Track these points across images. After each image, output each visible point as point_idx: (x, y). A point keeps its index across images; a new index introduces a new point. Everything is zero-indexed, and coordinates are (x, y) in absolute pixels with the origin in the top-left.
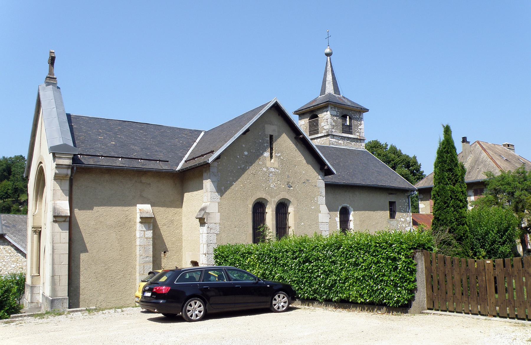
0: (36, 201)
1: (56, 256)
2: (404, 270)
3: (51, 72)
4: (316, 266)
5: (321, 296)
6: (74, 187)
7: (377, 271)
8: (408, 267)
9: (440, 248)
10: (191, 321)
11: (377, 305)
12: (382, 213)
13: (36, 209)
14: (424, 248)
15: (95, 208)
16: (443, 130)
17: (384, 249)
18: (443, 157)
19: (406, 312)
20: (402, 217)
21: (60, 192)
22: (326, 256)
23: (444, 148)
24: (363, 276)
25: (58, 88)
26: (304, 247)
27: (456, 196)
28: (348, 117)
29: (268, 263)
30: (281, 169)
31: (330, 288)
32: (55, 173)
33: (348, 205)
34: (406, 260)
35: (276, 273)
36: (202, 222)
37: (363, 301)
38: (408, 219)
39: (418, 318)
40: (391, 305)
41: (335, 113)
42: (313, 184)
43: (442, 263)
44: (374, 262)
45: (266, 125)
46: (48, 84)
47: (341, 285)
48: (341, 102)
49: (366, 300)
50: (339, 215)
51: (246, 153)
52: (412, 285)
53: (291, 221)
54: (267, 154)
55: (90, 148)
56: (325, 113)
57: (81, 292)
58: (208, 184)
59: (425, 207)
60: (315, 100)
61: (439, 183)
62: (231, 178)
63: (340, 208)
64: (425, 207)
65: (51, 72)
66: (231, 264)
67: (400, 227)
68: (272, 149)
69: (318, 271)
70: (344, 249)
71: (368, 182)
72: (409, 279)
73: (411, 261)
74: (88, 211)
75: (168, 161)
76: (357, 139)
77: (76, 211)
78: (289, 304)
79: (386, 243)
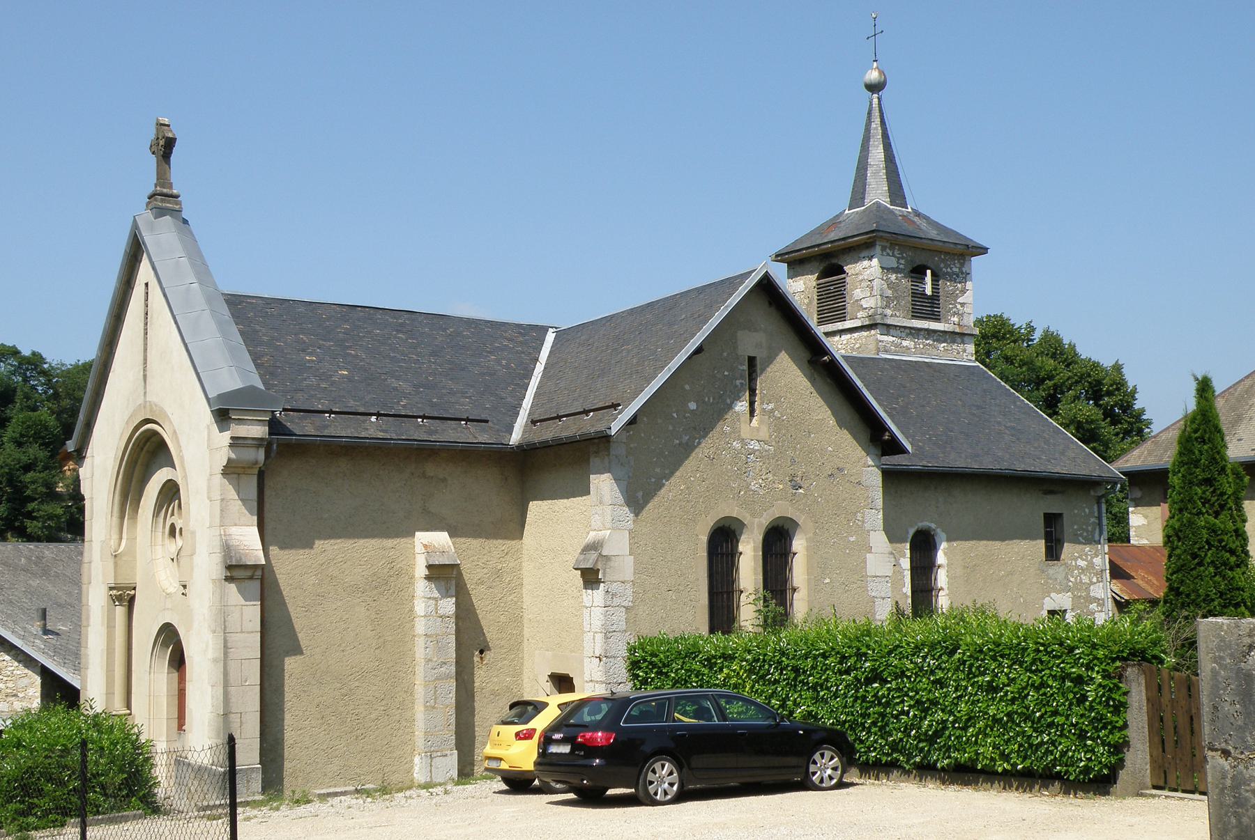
0: (122, 517)
1: (232, 665)
2: (1100, 703)
3: (163, 177)
4: (898, 689)
5: (909, 757)
6: (268, 493)
7: (1041, 704)
8: (1109, 698)
9: (1182, 656)
10: (655, 803)
11: (1041, 777)
12: (1025, 544)
13: (121, 538)
14: (1144, 659)
15: (317, 542)
16: (1192, 387)
17: (1054, 657)
18: (1192, 452)
19: (1106, 793)
20: (1080, 557)
21: (237, 506)
22: (921, 669)
23: (1196, 431)
24: (1009, 715)
25: (185, 222)
26: (868, 647)
27: (1221, 541)
28: (929, 272)
29: (776, 682)
30: (779, 446)
31: (931, 740)
32: (229, 460)
33: (933, 526)
34: (1105, 682)
35: (796, 704)
36: (591, 578)
37: (1009, 768)
38: (1097, 561)
39: (1131, 802)
40: (1072, 778)
41: (893, 262)
42: (852, 479)
43: (1184, 691)
44: (1033, 685)
45: (740, 334)
46: (160, 212)
47: (958, 733)
48: (908, 229)
49: (1014, 765)
50: (908, 552)
51: (692, 406)
52: (1118, 735)
53: (799, 572)
54: (742, 406)
55: (296, 390)
56: (866, 263)
57: (286, 754)
58: (603, 485)
59: (1146, 525)
60: (834, 223)
61: (1181, 510)
62: (658, 470)
63: (912, 532)
64: (1146, 525)
65: (163, 177)
66: (676, 683)
67: (1075, 583)
68: (753, 392)
69: (903, 701)
70: (964, 654)
71: (987, 463)
72: (1111, 723)
73: (1115, 685)
74: (301, 551)
75: (487, 421)
76: (953, 333)
77: (274, 550)
78: (843, 772)
79: (1061, 644)
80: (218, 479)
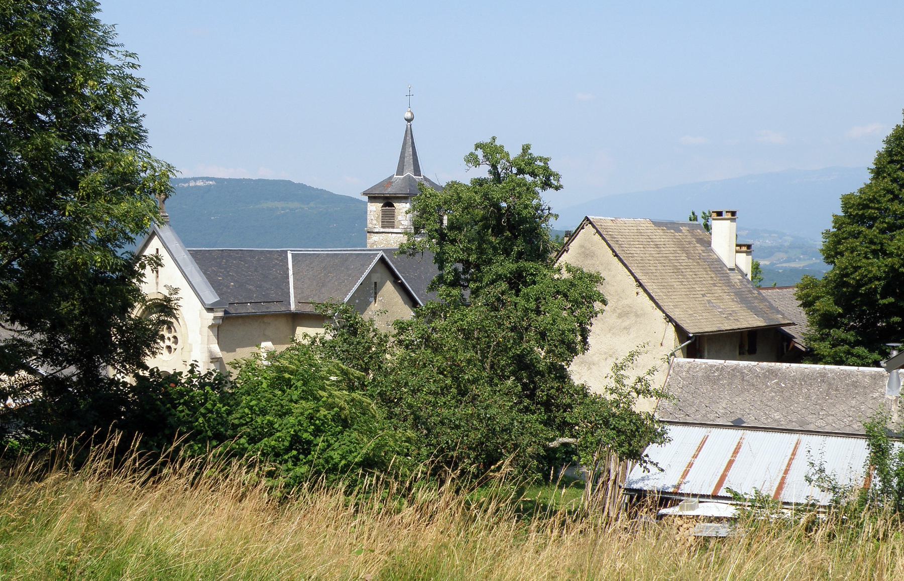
60: (389, 181)
80: (206, 329)
